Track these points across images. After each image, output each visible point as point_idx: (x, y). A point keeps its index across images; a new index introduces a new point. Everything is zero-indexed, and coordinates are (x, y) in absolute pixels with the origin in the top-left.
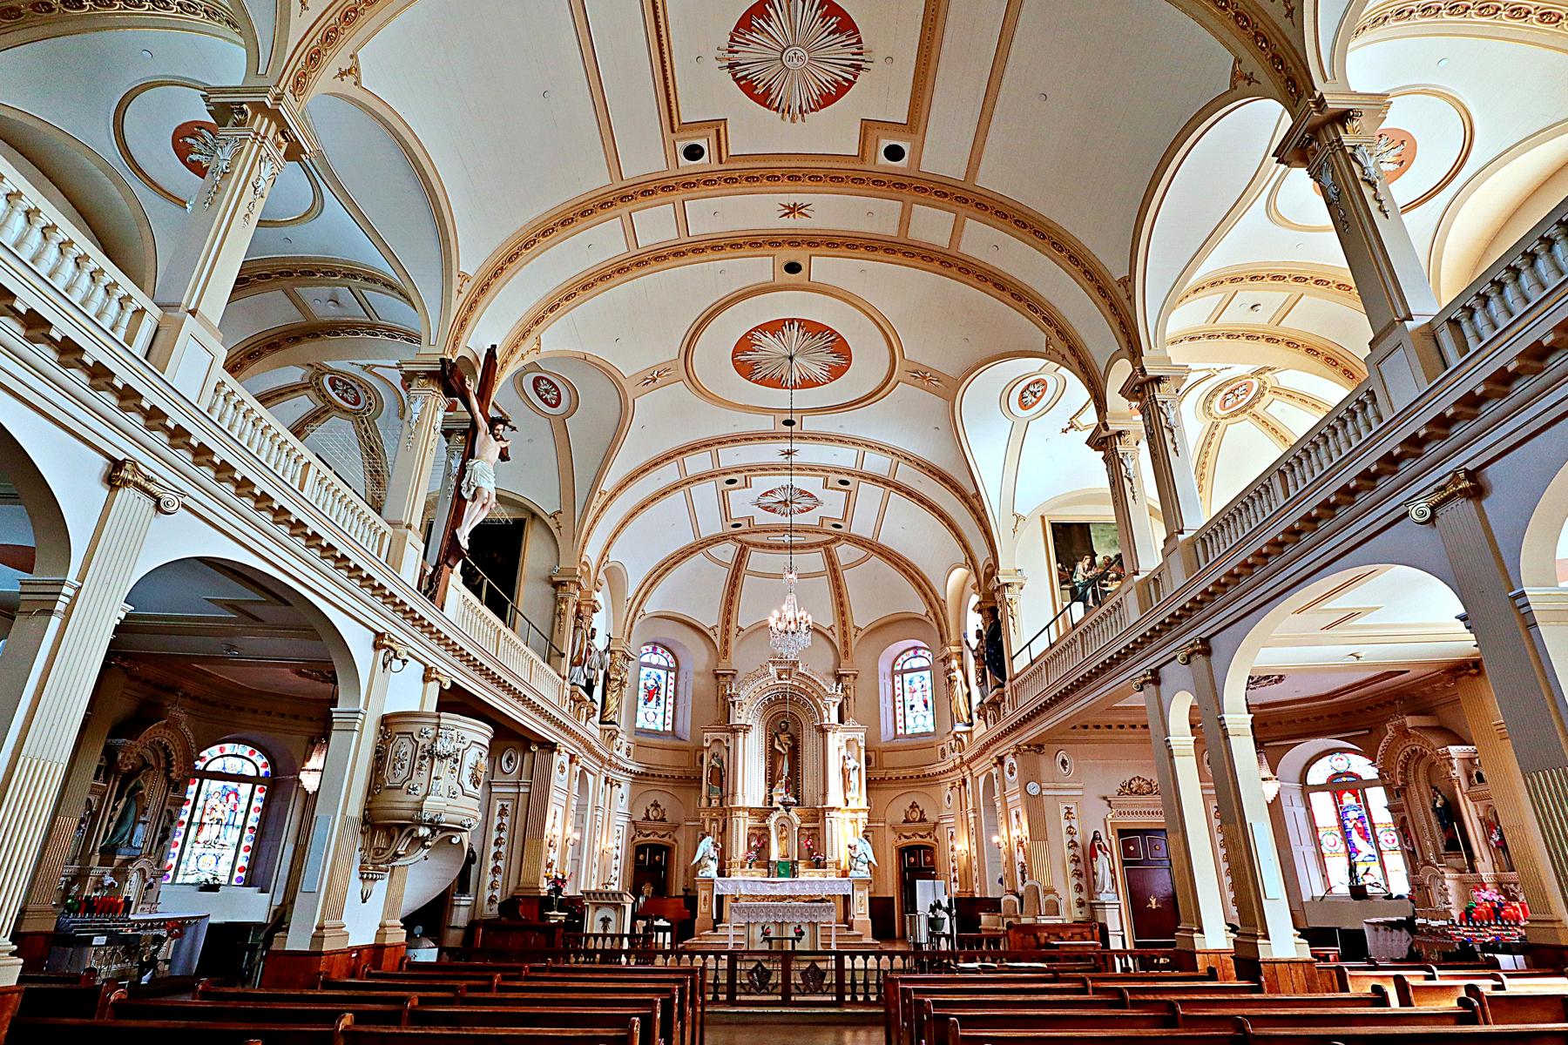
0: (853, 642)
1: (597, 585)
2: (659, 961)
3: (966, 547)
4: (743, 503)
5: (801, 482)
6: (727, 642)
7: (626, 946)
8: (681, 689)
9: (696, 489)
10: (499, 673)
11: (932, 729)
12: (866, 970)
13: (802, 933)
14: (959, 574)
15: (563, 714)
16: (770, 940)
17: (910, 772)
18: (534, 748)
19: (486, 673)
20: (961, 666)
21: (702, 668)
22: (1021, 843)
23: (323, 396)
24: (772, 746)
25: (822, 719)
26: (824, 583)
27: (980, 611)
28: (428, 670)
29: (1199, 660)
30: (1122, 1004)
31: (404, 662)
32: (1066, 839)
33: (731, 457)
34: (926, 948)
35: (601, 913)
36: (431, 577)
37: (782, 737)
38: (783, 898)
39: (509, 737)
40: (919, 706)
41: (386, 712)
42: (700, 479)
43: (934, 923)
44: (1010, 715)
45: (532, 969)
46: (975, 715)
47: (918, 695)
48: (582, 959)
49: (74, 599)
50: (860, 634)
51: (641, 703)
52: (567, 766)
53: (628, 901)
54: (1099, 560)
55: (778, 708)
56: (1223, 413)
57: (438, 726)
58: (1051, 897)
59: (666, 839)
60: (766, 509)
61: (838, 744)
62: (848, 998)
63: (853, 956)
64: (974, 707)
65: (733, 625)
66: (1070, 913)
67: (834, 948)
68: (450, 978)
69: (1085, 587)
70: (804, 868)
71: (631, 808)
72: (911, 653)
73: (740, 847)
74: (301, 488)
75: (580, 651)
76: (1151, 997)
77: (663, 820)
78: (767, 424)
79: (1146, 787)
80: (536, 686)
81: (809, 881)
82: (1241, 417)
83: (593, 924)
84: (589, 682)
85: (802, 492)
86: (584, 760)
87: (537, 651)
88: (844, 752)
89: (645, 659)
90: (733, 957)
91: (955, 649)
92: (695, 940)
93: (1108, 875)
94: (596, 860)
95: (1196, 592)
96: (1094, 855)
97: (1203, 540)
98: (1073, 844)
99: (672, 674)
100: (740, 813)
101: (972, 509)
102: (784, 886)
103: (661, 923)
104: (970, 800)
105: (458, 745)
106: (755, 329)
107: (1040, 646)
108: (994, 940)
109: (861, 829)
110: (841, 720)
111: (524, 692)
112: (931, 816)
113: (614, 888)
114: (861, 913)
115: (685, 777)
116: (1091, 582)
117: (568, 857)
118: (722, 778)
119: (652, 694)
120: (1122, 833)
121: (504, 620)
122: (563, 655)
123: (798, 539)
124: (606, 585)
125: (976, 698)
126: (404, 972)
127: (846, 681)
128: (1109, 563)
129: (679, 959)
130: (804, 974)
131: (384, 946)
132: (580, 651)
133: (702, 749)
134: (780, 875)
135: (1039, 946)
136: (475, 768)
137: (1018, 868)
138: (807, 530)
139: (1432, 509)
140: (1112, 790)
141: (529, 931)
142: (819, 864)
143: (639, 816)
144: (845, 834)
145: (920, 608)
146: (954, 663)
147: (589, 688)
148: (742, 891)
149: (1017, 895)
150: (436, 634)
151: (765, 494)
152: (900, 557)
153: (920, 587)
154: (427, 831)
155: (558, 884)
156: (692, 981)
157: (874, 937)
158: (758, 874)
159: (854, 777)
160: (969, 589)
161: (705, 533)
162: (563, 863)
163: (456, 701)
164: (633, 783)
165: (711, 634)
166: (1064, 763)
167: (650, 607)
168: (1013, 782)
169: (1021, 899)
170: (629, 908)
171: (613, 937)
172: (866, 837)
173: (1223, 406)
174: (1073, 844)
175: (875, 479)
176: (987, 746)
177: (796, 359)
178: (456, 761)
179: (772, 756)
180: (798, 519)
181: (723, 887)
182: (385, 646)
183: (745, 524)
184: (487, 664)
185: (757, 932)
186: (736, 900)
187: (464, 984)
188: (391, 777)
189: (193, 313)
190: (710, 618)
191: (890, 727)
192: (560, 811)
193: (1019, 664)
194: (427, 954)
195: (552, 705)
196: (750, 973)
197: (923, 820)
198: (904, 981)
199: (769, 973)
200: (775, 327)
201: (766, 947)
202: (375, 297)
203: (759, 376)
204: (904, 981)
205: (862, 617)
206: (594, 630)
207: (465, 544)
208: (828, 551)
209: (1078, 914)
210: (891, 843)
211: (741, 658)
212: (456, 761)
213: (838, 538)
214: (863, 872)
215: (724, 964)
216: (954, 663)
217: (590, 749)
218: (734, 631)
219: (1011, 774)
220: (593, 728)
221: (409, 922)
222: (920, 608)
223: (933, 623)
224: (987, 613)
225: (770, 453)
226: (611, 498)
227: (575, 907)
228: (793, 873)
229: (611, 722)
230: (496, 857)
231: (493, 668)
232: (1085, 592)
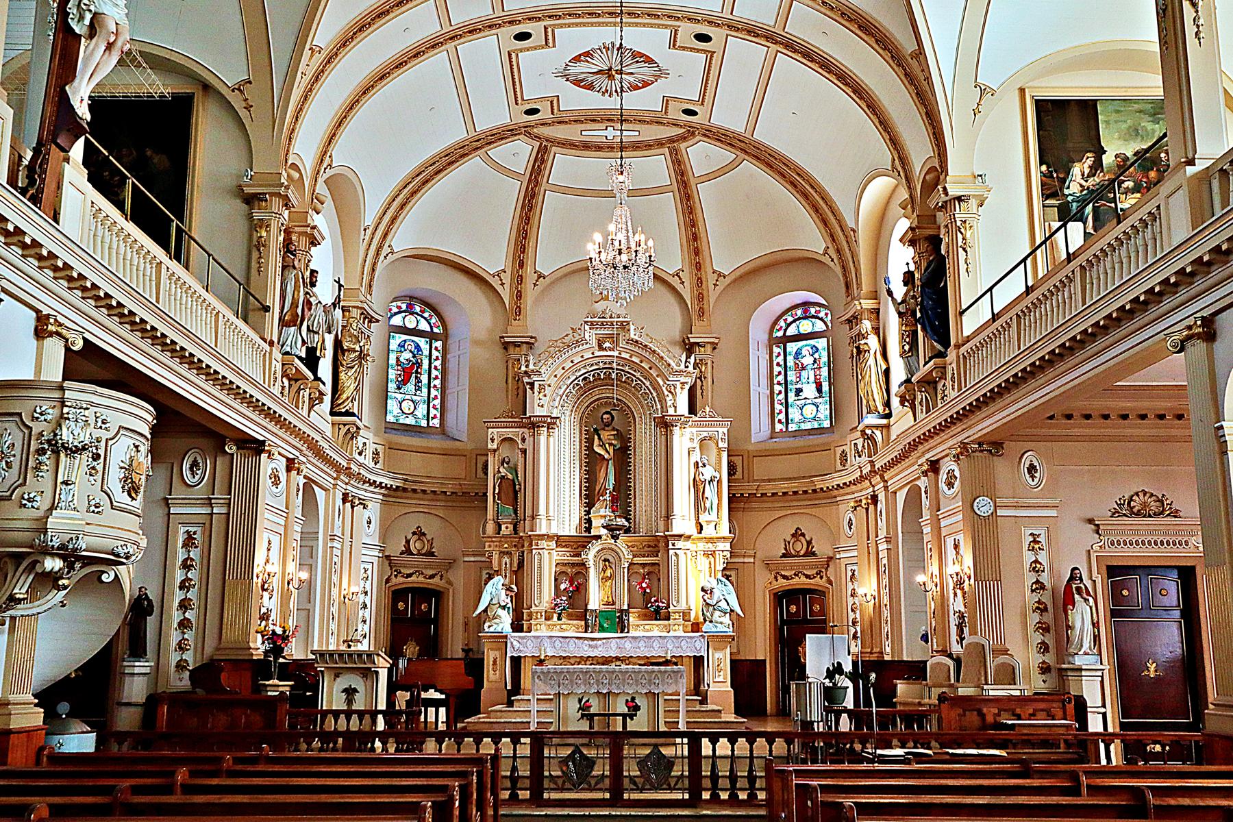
0: (712, 296)
1: (316, 203)
2: (430, 747)
3: (894, 142)
4: (542, 73)
5: (640, 38)
6: (519, 295)
7: (381, 725)
8: (452, 365)
9: (466, 48)
10: (162, 328)
11: (826, 424)
12: (732, 757)
13: (637, 708)
14: (880, 186)
15: (272, 396)
16: (590, 717)
17: (793, 486)
18: (230, 448)
19: (139, 327)
20: (877, 330)
21: (482, 335)
22: (959, 584)
24: (590, 448)
25: (664, 408)
26: (669, 204)
27: (912, 243)
28: (42, 319)
32: (1030, 578)
34: (819, 727)
35: (345, 681)
36: (31, 168)
37: (605, 435)
38: (607, 661)
39: (179, 428)
40: (809, 391)
42: (473, 30)
43: (831, 695)
44: (953, 398)
46: (895, 402)
47: (808, 375)
48: (316, 743)
50: (723, 283)
51: (392, 386)
52: (283, 475)
53: (382, 666)
54: (1108, 159)
55: (597, 394)
57: (63, 404)
58: (1002, 659)
59: (436, 580)
60: (577, 83)
62: (706, 795)
63: (714, 739)
64: (894, 389)
65: (529, 269)
66: (1031, 683)
67: (682, 727)
69: (1083, 202)
70: (630, 620)
71: (384, 537)
72: (799, 312)
73: (545, 593)
76: (1186, 802)
79: (1154, 506)
80: (233, 362)
81: (645, 637)
83: (331, 695)
84: (311, 352)
85: (636, 55)
86: (310, 467)
87: (227, 302)
88: (696, 456)
89: (397, 321)
90: (539, 740)
91: (868, 304)
92: (481, 717)
93: (1088, 626)
94: (334, 609)
96: (1069, 600)
98: (1040, 586)
99: (438, 344)
100: (543, 544)
101: (910, 78)
102: (609, 645)
103: (432, 694)
104: (882, 525)
105: (98, 433)
107: (1014, 287)
108: (914, 717)
109: (720, 567)
110: (692, 410)
111: (207, 360)
112: (822, 548)
113: (364, 646)
114: (719, 681)
115: (462, 490)
116: (1094, 195)
117: (292, 605)
118: (515, 493)
119: (409, 372)
120: (1112, 571)
121: (165, 245)
122: (266, 309)
123: (631, 134)
124: (329, 202)
125: (899, 373)
126: (45, 766)
127: (700, 353)
128: (1123, 165)
129: (459, 744)
130: (642, 763)
132: (294, 304)
133: (485, 453)
134: (602, 629)
135: (985, 726)
136: (129, 468)
137: (954, 620)
138: (643, 119)
140: (1102, 511)
141: (246, 705)
142: (658, 614)
143: (396, 548)
144: (695, 576)
145: (814, 241)
146: (867, 325)
147: (312, 360)
148: (550, 652)
149: (950, 656)
150: (48, 260)
151: (577, 59)
152: (787, 162)
153: (816, 210)
155: (277, 642)
156: (480, 775)
157: (738, 712)
158: (571, 628)
159: (710, 492)
160: (895, 209)
161: (485, 123)
162: (285, 615)
163: (90, 365)
164: (384, 503)
165: (495, 283)
166: (1032, 469)
167: (402, 241)
168: (952, 499)
169: (958, 661)
170: (383, 674)
171: (361, 714)
172: (727, 577)
174: (1040, 586)
175: (752, 31)
176: (913, 446)
179: (591, 462)
180: (634, 101)
181: (519, 645)
183: (545, 108)
184: (141, 313)
185: (572, 707)
186: (541, 662)
187: (127, 783)
190: (493, 259)
191: (765, 420)
192: (276, 540)
193: (970, 324)
194: (79, 741)
195: (253, 383)
196: (564, 761)
197: (810, 553)
198: (799, 774)
199: (591, 763)
201: (584, 726)
204: (799, 774)
205: (724, 258)
206: (313, 272)
207: (83, 111)
208: (675, 153)
209: (1039, 683)
210: (764, 585)
211: (543, 319)
212: (96, 457)
214: (723, 624)
215: (525, 749)
216: (867, 325)
217: (318, 452)
218: (530, 277)
219: (950, 485)
221: (47, 697)
222: (814, 241)
223: (838, 262)
224: (924, 246)
227: (305, 676)
228: (622, 626)
229: (349, 414)
230: (184, 605)
231: (152, 321)
232: (1081, 210)
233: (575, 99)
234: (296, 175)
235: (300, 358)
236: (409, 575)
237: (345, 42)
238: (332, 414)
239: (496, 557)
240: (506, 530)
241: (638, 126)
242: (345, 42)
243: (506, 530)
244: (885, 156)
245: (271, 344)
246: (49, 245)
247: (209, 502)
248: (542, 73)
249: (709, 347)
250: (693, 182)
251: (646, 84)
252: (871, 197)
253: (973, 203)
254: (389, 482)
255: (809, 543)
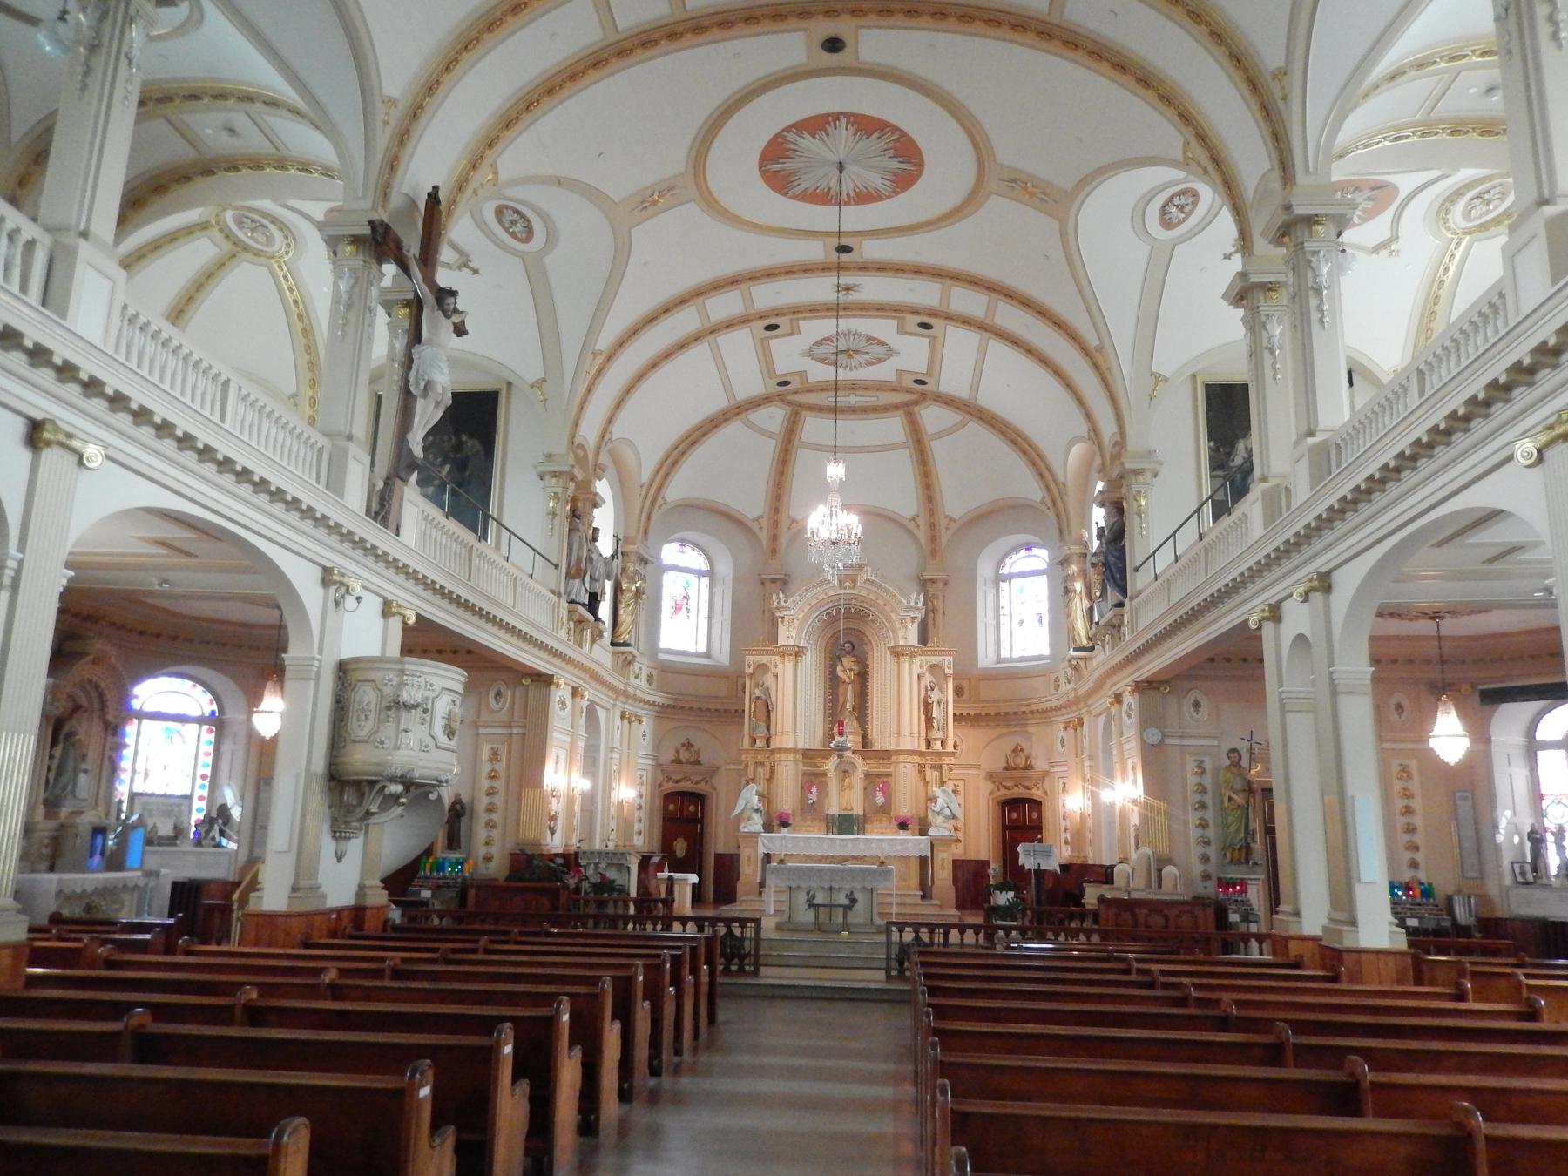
0: (944, 538)
3: (1089, 417)
4: (790, 354)
7: (632, 911)
9: (726, 340)
14: (1077, 452)
23: (228, 236)
29: (1317, 597)
30: (1151, 985)
31: (359, 599)
33: (768, 296)
41: (346, 654)
42: (729, 325)
44: (1132, 639)
45: (522, 934)
49: (18, 572)
50: (954, 527)
52: (569, 701)
56: (1463, 224)
61: (917, 670)
68: (435, 941)
74: (222, 418)
75: (579, 560)
77: (698, 763)
78: (816, 251)
82: (1493, 230)
95: (1321, 509)
97: (1338, 446)
101: (1096, 367)
106: (788, 129)
110: (924, 639)
124: (611, 470)
131: (364, 908)
132: (579, 560)
136: (449, 717)
138: (880, 387)
139: (1540, 451)
143: (667, 756)
147: (593, 603)
150: (393, 564)
154: (400, 788)
163: (425, 641)
165: (755, 527)
166: (1197, 705)
173: (1467, 214)
177: (849, 168)
178: (425, 711)
182: (335, 583)
185: (802, 898)
188: (360, 728)
189: (84, 235)
190: (752, 505)
192: (563, 754)
195: (541, 630)
200: (817, 125)
202: (281, 124)
203: (798, 190)
206: (596, 530)
207: (418, 452)
212: (425, 711)
213: (923, 398)
220: (601, 655)
222: (1032, 490)
225: (821, 289)
226: (609, 359)
229: (626, 644)
233: (820, 373)
234: (581, 453)
235: (584, 605)
236: (678, 781)
237: (621, 344)
238: (613, 644)
239: (751, 768)
240: (760, 744)
241: (874, 393)
242: (621, 344)
243: (760, 744)
244: (1083, 428)
245: (559, 595)
246: (394, 552)
247: (510, 725)
248: (790, 354)
249: (941, 585)
250: (926, 439)
251: (880, 361)
252: (1071, 459)
253: (1148, 475)
254: (657, 700)
255: (1027, 758)
